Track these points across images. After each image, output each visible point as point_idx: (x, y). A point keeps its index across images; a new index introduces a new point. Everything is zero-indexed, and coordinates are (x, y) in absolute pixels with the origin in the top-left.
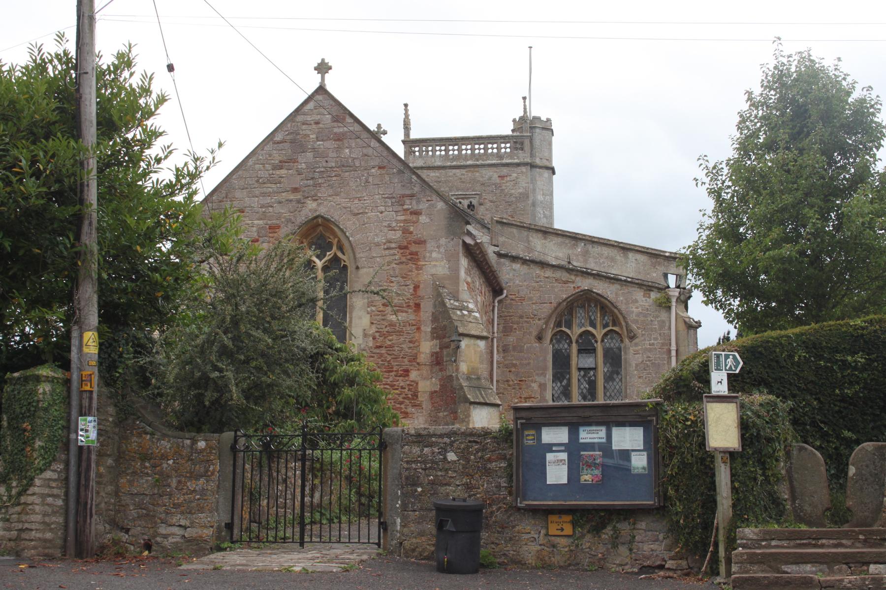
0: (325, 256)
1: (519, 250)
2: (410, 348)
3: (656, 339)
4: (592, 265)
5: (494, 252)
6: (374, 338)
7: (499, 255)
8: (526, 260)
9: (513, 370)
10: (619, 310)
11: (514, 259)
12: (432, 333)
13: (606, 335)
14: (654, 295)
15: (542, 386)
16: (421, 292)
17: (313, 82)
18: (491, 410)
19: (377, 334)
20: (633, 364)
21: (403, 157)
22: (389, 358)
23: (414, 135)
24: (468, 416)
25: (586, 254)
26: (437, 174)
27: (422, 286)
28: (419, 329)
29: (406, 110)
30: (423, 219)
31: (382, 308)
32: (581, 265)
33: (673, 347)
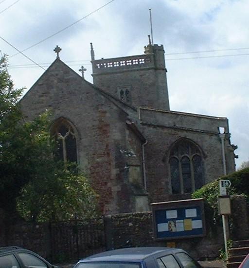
0: (65, 134)
1: (151, 120)
2: (107, 172)
3: (216, 157)
4: (185, 126)
5: (141, 123)
6: (90, 170)
7: (143, 124)
8: (155, 126)
9: (153, 176)
10: (199, 145)
11: (150, 125)
12: (116, 165)
13: (194, 157)
14: (214, 137)
15: (167, 183)
16: (109, 148)
17: (52, 58)
18: (146, 197)
19: (92, 168)
20: (207, 169)
21: (92, 83)
22: (98, 178)
23: (96, 58)
24: (135, 201)
25: (181, 121)
26: (109, 77)
27: (109, 145)
28: (110, 164)
29: (92, 46)
30: (108, 115)
31: (92, 156)
32: (180, 126)
33: (224, 160)
